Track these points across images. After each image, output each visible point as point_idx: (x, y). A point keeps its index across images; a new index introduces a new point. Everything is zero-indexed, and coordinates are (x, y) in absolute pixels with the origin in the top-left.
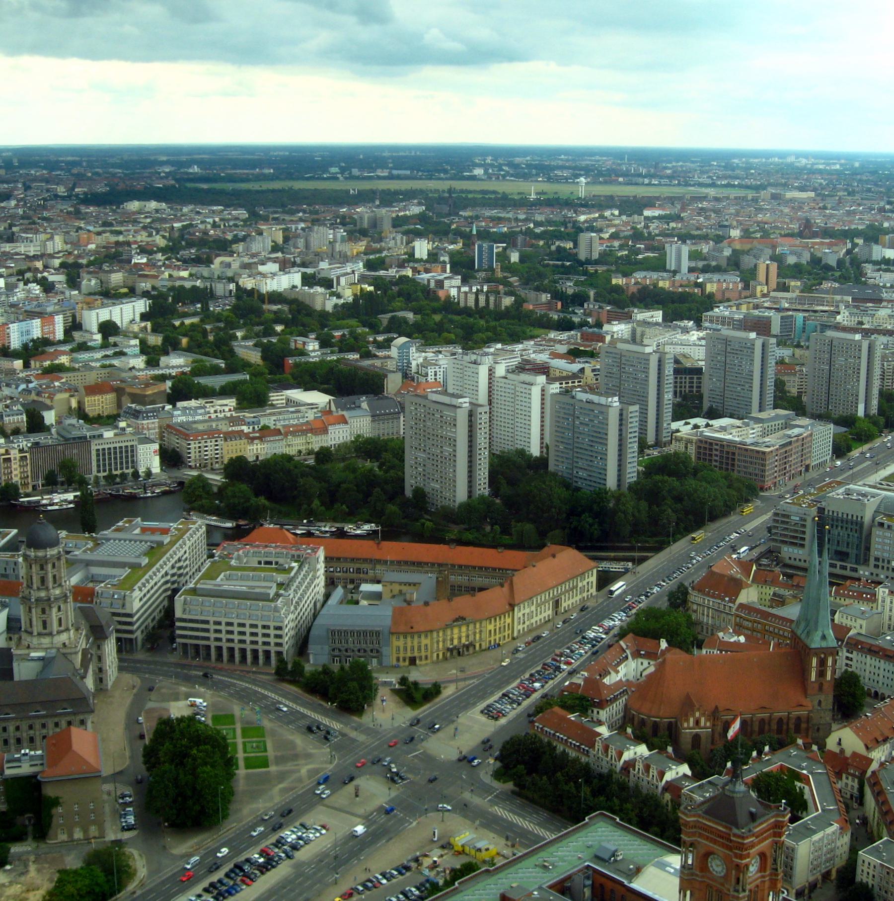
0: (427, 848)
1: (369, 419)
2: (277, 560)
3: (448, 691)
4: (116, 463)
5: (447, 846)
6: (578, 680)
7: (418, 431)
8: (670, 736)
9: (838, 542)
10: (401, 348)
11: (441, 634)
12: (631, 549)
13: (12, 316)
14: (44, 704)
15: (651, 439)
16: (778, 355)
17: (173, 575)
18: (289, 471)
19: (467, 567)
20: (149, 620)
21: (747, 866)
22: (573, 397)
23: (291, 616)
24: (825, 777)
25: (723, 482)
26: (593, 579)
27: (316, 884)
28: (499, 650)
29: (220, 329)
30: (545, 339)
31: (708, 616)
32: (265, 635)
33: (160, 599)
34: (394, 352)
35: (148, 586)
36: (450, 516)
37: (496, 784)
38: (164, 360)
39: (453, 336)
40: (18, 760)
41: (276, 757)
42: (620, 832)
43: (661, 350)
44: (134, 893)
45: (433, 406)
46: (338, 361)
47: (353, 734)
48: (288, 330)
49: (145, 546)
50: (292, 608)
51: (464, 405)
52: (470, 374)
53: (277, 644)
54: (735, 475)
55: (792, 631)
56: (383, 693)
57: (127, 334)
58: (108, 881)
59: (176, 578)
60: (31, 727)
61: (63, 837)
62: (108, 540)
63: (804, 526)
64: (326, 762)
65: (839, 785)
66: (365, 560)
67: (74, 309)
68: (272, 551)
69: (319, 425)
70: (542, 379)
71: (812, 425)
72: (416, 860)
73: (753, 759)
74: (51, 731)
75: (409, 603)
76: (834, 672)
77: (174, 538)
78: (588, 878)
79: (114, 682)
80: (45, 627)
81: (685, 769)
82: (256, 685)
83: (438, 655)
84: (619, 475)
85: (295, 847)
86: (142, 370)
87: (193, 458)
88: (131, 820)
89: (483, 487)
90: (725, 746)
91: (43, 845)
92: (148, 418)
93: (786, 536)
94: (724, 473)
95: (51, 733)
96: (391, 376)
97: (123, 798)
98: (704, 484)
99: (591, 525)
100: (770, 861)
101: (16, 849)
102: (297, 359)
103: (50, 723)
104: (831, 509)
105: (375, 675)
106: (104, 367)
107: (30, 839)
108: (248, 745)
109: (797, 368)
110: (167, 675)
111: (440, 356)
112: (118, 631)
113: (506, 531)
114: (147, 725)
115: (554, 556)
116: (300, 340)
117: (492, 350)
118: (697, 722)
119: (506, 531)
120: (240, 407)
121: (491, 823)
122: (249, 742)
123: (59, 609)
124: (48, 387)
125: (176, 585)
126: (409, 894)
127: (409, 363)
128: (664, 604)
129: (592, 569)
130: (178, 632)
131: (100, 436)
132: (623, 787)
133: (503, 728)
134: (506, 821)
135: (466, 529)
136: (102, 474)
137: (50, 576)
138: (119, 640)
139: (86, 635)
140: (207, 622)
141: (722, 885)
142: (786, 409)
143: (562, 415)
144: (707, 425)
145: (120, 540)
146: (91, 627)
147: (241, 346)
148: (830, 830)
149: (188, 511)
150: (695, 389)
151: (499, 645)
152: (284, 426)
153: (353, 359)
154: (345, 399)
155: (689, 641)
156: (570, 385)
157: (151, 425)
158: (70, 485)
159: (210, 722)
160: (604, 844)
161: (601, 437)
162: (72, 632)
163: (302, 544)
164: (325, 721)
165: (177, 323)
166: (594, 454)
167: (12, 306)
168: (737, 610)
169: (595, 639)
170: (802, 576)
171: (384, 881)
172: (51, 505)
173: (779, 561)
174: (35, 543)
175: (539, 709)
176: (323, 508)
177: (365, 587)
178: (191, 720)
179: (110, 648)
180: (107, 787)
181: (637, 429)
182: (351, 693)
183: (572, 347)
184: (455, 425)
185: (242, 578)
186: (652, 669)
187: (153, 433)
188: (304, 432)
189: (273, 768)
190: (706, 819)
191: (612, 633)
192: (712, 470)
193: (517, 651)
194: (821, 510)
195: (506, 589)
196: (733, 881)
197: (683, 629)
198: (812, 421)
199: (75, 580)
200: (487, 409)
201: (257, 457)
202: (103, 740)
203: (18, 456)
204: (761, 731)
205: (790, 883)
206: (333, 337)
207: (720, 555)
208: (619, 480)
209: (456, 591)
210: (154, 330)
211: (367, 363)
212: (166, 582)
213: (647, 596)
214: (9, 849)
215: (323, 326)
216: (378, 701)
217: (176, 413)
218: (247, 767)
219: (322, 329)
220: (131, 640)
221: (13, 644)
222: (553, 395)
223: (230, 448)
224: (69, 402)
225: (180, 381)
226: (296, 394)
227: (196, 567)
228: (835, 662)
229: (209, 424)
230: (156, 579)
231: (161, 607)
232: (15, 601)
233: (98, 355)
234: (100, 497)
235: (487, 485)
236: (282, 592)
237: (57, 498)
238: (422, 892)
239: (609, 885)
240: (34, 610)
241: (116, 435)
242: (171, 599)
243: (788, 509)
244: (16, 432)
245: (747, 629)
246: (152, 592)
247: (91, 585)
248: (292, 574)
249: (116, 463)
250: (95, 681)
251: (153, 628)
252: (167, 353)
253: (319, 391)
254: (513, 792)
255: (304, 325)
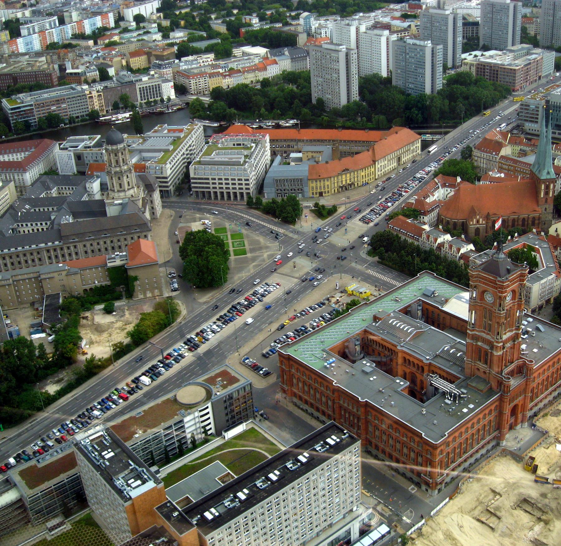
0: (333, 293)
1: (290, 61)
2: (244, 142)
3: (341, 210)
4: (151, 95)
5: (344, 291)
6: (412, 200)
7: (317, 66)
8: (463, 229)
9: (557, 120)
10: (306, 18)
11: (336, 179)
12: (440, 127)
13: (85, 15)
14: (125, 228)
15: (450, 64)
16: (523, 12)
17: (187, 155)
18: (247, 93)
19: (348, 141)
20: (177, 180)
21: (505, 297)
22: (405, 42)
23: (253, 173)
24: (548, 249)
25: (492, 88)
26: (419, 145)
27: (275, 314)
28: (368, 186)
29: (202, 14)
30: (387, 9)
31: (483, 163)
32: (220, 184)
33: (181, 167)
34: (301, 21)
35: (174, 161)
36: (337, 113)
37: (370, 258)
38: (172, 34)
39: (334, 10)
40: (114, 258)
41: (250, 249)
42: (436, 281)
43: (455, 12)
44: (181, 323)
45: (325, 51)
46: (270, 28)
47: (291, 235)
48: (240, 12)
49: (171, 140)
50: (254, 169)
51: (343, 50)
52: (345, 31)
53: (247, 189)
54: (499, 83)
55: (531, 170)
56: (306, 212)
57: (150, 21)
58: (167, 318)
59: (189, 156)
60: (119, 241)
61: (141, 296)
62: (150, 137)
63: (538, 111)
64: (277, 250)
65: (555, 254)
66: (292, 140)
67: (119, 8)
68: (240, 138)
69: (261, 66)
70: (386, 32)
71: (543, 53)
72: (328, 299)
73: (509, 241)
74: (129, 242)
75: (317, 163)
76: (554, 192)
77: (186, 134)
78: (420, 306)
79: (161, 214)
80: (121, 187)
81: (471, 247)
82: (238, 212)
83: (335, 190)
84: (432, 86)
85: (263, 296)
86: (160, 41)
87: (193, 89)
88: (176, 285)
89: (355, 96)
90: (493, 234)
91: (131, 301)
92: (166, 68)
93: (527, 117)
94: (492, 82)
95: (129, 243)
96: (301, 36)
97: (170, 275)
98: (481, 89)
99: (417, 115)
100: (517, 295)
101: (117, 304)
102: (247, 29)
103: (129, 238)
104: (553, 101)
105: (301, 203)
106: (138, 41)
107: (124, 299)
108: (236, 244)
109: (534, 19)
110: (189, 209)
111: (328, 22)
112: (160, 187)
113: (369, 120)
114: (181, 237)
115: (397, 133)
116: (248, 17)
117: (357, 17)
118: (478, 221)
119: (369, 120)
120: (217, 58)
121: (367, 279)
122: (235, 242)
123: (127, 177)
124: (109, 54)
125: (189, 160)
126: (325, 317)
127: (310, 27)
128: (459, 157)
129: (418, 139)
130: (193, 185)
131: (141, 80)
132: (438, 257)
133: (371, 228)
134: (375, 277)
135: (346, 120)
136: (143, 101)
137: (121, 159)
138: (161, 191)
139: (143, 190)
140: (208, 179)
141: (492, 307)
142: (527, 44)
143: (398, 53)
144: (482, 55)
145: (157, 137)
146: (146, 185)
147: (215, 24)
148: (550, 277)
149: (193, 119)
150: (475, 34)
151: (368, 183)
152: (242, 68)
153: (279, 27)
154: (275, 50)
155: (473, 177)
156: (403, 35)
157: (168, 72)
158: (126, 109)
159: (213, 232)
160: (428, 288)
161: (421, 64)
162: (135, 189)
163: (257, 133)
164: (275, 228)
165: (177, 13)
166: (418, 75)
167: (84, 9)
168: (500, 159)
169: (421, 178)
170: (537, 139)
171: (311, 311)
172: (117, 120)
173: (523, 132)
174: (111, 142)
175: (390, 217)
176: (267, 112)
177: (293, 155)
178: (204, 232)
179: (157, 195)
180: (162, 269)
181: (442, 59)
182: (289, 213)
183: (403, 13)
184: (338, 61)
185: (225, 154)
186: (453, 193)
187: (170, 76)
188: (254, 71)
189: (249, 255)
190: (483, 273)
191: (430, 174)
192: (485, 81)
193: (378, 186)
194: (547, 102)
195: (370, 152)
196: (498, 305)
197: (470, 171)
198: (543, 50)
199: (134, 160)
200: (356, 51)
201: (228, 86)
202: (158, 245)
203: (97, 94)
204: (513, 225)
205: (529, 305)
206: (266, 15)
207: (490, 129)
208: (432, 89)
209: (343, 155)
210: (165, 18)
211: (286, 28)
212: (184, 159)
213: (449, 153)
214: (114, 304)
215: (260, 9)
216: (303, 216)
217: (181, 64)
218: (235, 255)
219: (260, 10)
220: (167, 191)
221: (105, 197)
222: (393, 41)
223: (213, 82)
224: (121, 62)
225: (182, 46)
226: (248, 49)
227: (200, 149)
228: (554, 186)
229: (200, 69)
230: (178, 157)
231: (182, 172)
232: (103, 174)
233: (135, 34)
234: (144, 114)
235: (358, 95)
236: (247, 160)
237: (120, 116)
238: (331, 316)
239: (431, 309)
240: (114, 178)
241: (149, 79)
242: (187, 167)
243: (529, 102)
244: (94, 81)
245: (505, 169)
246: (177, 164)
247: (143, 163)
248: (252, 150)
249: (151, 95)
250: (150, 214)
251: (179, 184)
252: (173, 30)
253: (261, 46)
254: (378, 262)
255: (249, 9)
